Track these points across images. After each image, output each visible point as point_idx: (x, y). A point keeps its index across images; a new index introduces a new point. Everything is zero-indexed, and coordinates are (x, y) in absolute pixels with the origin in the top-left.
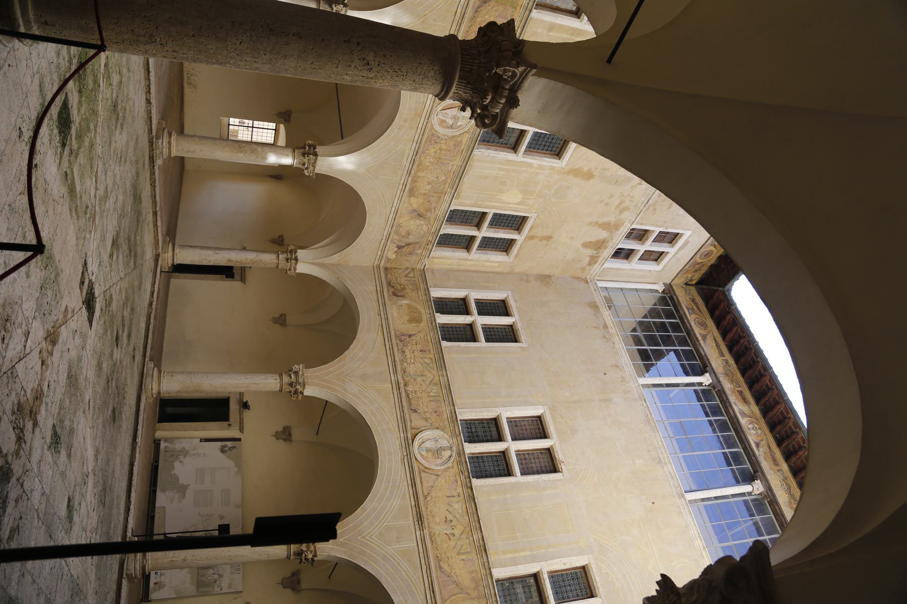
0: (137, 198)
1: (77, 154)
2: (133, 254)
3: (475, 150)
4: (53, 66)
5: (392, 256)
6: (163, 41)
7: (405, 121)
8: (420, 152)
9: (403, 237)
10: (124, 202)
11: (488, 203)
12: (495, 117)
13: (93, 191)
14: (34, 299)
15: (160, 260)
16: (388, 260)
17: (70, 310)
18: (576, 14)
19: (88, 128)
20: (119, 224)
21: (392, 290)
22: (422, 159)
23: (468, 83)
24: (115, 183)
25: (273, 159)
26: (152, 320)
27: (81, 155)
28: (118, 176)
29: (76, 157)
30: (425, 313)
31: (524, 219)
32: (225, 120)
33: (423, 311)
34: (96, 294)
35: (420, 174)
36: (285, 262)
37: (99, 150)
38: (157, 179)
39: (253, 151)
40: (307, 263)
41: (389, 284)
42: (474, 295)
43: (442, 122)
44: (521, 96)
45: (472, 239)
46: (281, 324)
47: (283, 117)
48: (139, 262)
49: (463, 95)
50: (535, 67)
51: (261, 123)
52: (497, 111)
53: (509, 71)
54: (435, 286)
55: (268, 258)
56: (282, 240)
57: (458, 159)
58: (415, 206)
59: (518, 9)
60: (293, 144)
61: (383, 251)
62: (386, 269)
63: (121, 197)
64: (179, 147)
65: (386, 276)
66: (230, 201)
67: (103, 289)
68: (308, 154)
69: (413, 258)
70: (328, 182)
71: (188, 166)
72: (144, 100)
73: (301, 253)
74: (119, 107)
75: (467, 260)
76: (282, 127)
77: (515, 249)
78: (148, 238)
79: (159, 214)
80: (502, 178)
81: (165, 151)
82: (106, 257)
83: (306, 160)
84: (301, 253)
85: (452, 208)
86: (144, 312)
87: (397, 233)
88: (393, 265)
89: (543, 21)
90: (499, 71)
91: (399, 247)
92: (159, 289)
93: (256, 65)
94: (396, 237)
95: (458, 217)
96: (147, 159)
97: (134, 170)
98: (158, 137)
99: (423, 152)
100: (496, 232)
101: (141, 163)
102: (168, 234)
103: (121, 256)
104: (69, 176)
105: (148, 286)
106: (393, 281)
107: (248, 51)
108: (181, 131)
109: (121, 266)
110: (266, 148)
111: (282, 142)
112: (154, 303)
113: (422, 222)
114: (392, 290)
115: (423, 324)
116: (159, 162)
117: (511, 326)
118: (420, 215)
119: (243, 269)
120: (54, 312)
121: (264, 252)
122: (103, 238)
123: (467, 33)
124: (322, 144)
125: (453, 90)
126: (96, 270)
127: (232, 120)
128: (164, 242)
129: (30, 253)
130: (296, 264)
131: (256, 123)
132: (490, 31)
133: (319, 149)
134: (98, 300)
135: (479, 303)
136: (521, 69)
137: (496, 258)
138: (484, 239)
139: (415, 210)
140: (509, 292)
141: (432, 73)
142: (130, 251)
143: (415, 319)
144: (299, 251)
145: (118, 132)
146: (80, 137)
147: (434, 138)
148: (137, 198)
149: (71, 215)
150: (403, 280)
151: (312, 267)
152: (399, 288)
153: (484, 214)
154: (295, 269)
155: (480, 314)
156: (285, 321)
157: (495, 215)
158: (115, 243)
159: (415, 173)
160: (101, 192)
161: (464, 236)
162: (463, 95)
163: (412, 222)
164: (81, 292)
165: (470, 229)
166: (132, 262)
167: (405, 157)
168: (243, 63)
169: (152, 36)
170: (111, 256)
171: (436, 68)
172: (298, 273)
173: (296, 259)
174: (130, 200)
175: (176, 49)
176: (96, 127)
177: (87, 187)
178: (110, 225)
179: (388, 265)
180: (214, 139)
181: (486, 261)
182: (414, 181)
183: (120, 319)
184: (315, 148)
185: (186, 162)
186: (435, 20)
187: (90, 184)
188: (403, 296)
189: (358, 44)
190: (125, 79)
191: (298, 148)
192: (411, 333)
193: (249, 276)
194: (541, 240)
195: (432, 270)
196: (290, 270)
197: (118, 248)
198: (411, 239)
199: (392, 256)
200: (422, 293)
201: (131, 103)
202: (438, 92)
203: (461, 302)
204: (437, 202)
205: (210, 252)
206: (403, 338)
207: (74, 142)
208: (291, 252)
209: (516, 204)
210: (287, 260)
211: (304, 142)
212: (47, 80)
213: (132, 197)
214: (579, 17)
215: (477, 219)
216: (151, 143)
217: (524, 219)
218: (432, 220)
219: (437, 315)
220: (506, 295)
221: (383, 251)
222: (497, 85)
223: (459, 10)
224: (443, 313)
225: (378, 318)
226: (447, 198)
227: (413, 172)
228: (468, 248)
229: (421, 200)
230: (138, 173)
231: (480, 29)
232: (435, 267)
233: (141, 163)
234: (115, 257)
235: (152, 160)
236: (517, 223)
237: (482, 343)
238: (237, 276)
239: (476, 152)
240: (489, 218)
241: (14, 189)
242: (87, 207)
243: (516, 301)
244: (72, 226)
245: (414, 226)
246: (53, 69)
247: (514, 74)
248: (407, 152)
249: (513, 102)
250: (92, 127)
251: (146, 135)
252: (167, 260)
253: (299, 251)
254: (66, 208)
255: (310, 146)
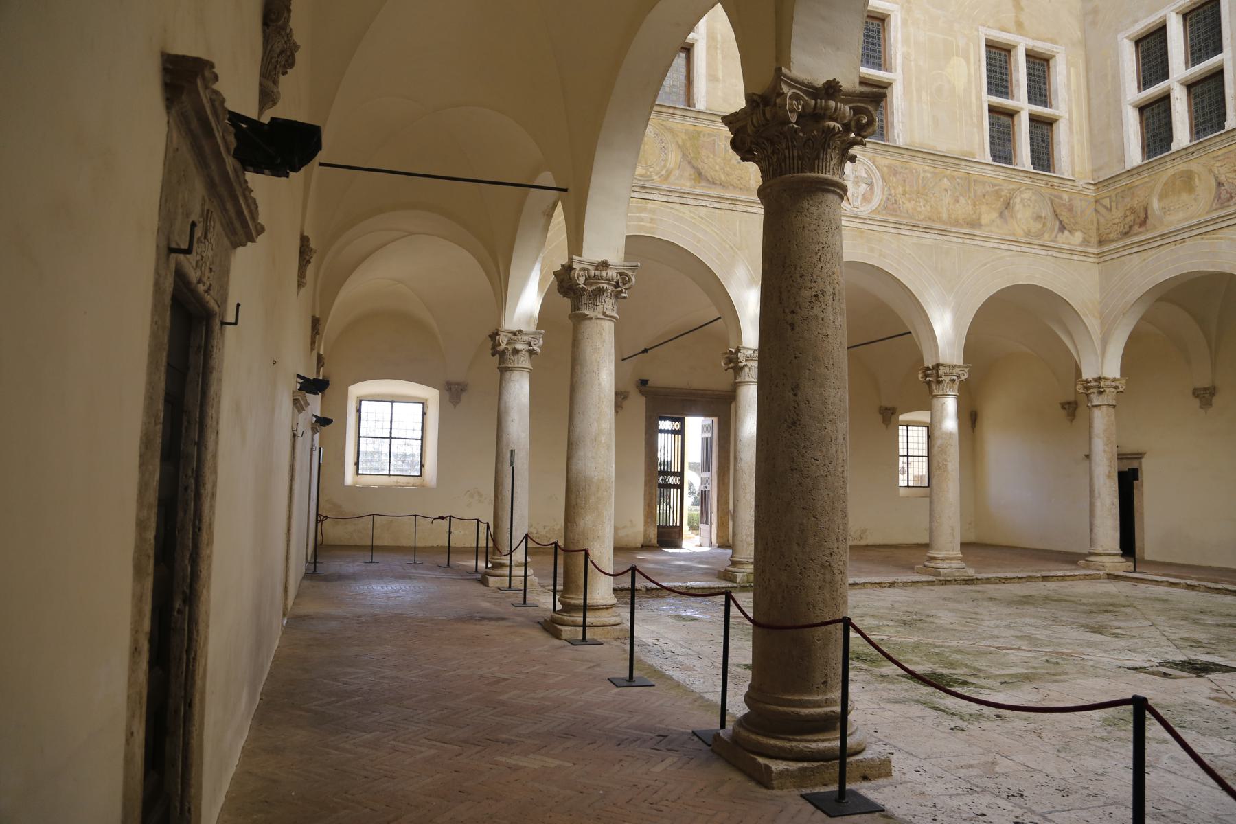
0: (1026, 601)
1: (974, 668)
2: (1110, 608)
3: (897, 144)
4: (868, 687)
5: (1079, 236)
6: (827, 552)
7: (872, 250)
8: (913, 222)
9: (1044, 224)
10: (1034, 617)
11: (974, 108)
12: (857, 111)
13: (1022, 653)
14: (1202, 738)
15: (1116, 573)
16: (1085, 242)
17: (1215, 695)
18: (688, 49)
19: (937, 654)
20: (1067, 623)
21: (1136, 228)
22: (922, 217)
23: (817, 158)
24: (1008, 627)
25: (950, 423)
26: (1219, 586)
27: (976, 664)
28: (998, 622)
29: (980, 670)
30: (1170, 169)
31: (991, 46)
32: (902, 492)
33: (1171, 172)
34: (1184, 658)
35: (945, 216)
36: (1105, 396)
37: (965, 644)
38: (994, 575)
39: (943, 450)
40: (1104, 362)
41: (1126, 234)
42: (1132, 93)
43: (866, 199)
44: (820, 81)
45: (1034, 119)
46: (1213, 394)
47: (889, 416)
48: (1122, 600)
49: (835, 161)
50: (778, 70)
51: (901, 445)
52: (847, 108)
53: (791, 104)
54: (1122, 160)
55: (1101, 420)
56: (1069, 403)
57: (914, 166)
58: (995, 215)
59: (699, 129)
60: (925, 398)
61: (1071, 252)
62: (1101, 243)
63: (1027, 621)
64: (948, 547)
65: (1113, 241)
66: (1015, 479)
67: (1173, 649)
68: (938, 376)
69: (1079, 204)
70: (973, 346)
71: (972, 537)
72: (890, 590)
73: (1088, 374)
74: (904, 618)
75: (1070, 120)
76: (902, 418)
77: (1042, 47)
78: (1083, 588)
79: (1045, 574)
80: (933, 95)
81: (955, 564)
82: (1121, 643)
83: (947, 379)
84: (1088, 374)
85: (989, 160)
86: (1207, 596)
87: (1040, 235)
88: (1094, 233)
89: (708, 92)
90: (793, 118)
91: (1063, 228)
92: (1163, 575)
93: (840, 438)
94: (1046, 236)
95: (1002, 148)
96: (968, 587)
97: (987, 603)
98: (939, 574)
99: (912, 217)
100: (1018, 85)
101: (976, 595)
102: (1074, 562)
103: (1117, 624)
104: (1007, 679)
105: (1161, 591)
106: (1121, 229)
107: (824, 449)
108: (926, 546)
109: (1133, 624)
110: (937, 434)
111: (924, 416)
112: (1189, 582)
113: (1018, 200)
114: (1136, 228)
115: (1194, 166)
116: (971, 572)
117: (1185, 16)
118: (1008, 205)
119: (1121, 457)
120: (1222, 715)
121: (1090, 426)
122: (1090, 644)
123: (752, 173)
124: (921, 360)
125: (830, 176)
126: (1144, 657)
127: (902, 482)
128: (1087, 567)
129: (1148, 714)
130: (1106, 379)
131: (902, 451)
132: (743, 146)
133: (929, 363)
134: (1193, 657)
135: (1144, 83)
136: (785, 89)
137: (1062, 76)
138: (1032, 99)
139: (1001, 215)
140: (1120, 36)
141: (813, 209)
142: (1107, 611)
143: (1187, 181)
144: (1084, 377)
145: (937, 621)
146: (952, 665)
147: (890, 206)
148: (1026, 601)
149: (1062, 681)
150: (1117, 214)
151: (1109, 355)
152: (1131, 218)
153: (992, 109)
154: (1115, 380)
155: (1166, 76)
156: (1205, 389)
157: (990, 92)
158: (1097, 630)
159: (945, 223)
160: (1024, 644)
161: (1031, 132)
162: (835, 161)
163: (1019, 216)
164: (1176, 678)
165: (1019, 126)
166: (1123, 609)
167: (923, 241)
168: (841, 456)
169: (823, 566)
170: (1117, 636)
171: (806, 205)
172: (1122, 375)
173: (1099, 379)
174: (1030, 609)
175: (834, 537)
176: (936, 646)
177: (1019, 660)
178: (1070, 636)
179: (1094, 240)
180: (931, 502)
181: (1069, 89)
182: (956, 223)
183: (1222, 629)
184: (928, 369)
185: (966, 541)
186: (735, 235)
187: (1013, 656)
188: (1146, 210)
189: (793, 312)
190: (869, 611)
191: (931, 391)
192: (1213, 183)
193: (1131, 447)
194: (1022, 9)
195: (1094, 171)
196: (1116, 387)
197: (1105, 627)
198: (1047, 212)
199: (1079, 236)
200: (1137, 180)
201: (897, 605)
202: (836, 197)
203: (1147, 113)
204: (984, 183)
205: (1098, 504)
206: (1224, 196)
207: (958, 671)
208: (1087, 388)
209: (968, 62)
210: (1101, 393)
211: (928, 382)
212: (886, 695)
213: (1026, 607)
214: (692, 45)
215: (1001, 118)
216: (946, 582)
217: (991, 46)
218: (1012, 186)
219: (1175, 147)
220: (1126, 42)
221: (1071, 252)
222: (813, 117)
223: (717, 205)
224: (1169, 138)
225: (1189, 243)
226: (975, 170)
227: (944, 227)
228: (1049, 123)
229: (984, 208)
230: (990, 599)
231: (743, 159)
232: (1088, 167)
233: (976, 595)
234: (1119, 631)
235: (969, 581)
236: (998, 54)
237: (1225, 58)
238: (1135, 464)
239: (900, 142)
240: (998, 100)
241: (1034, 743)
242: (1047, 661)
243: (1136, 21)
244: (1079, 681)
245: (1024, 215)
246: (871, 687)
247: (795, 97)
248: (915, 240)
249: (832, 89)
250: (936, 650)
251: (936, 588)
252: (1119, 565)
253: (1084, 377)
254: (1053, 686)
255: (926, 376)
